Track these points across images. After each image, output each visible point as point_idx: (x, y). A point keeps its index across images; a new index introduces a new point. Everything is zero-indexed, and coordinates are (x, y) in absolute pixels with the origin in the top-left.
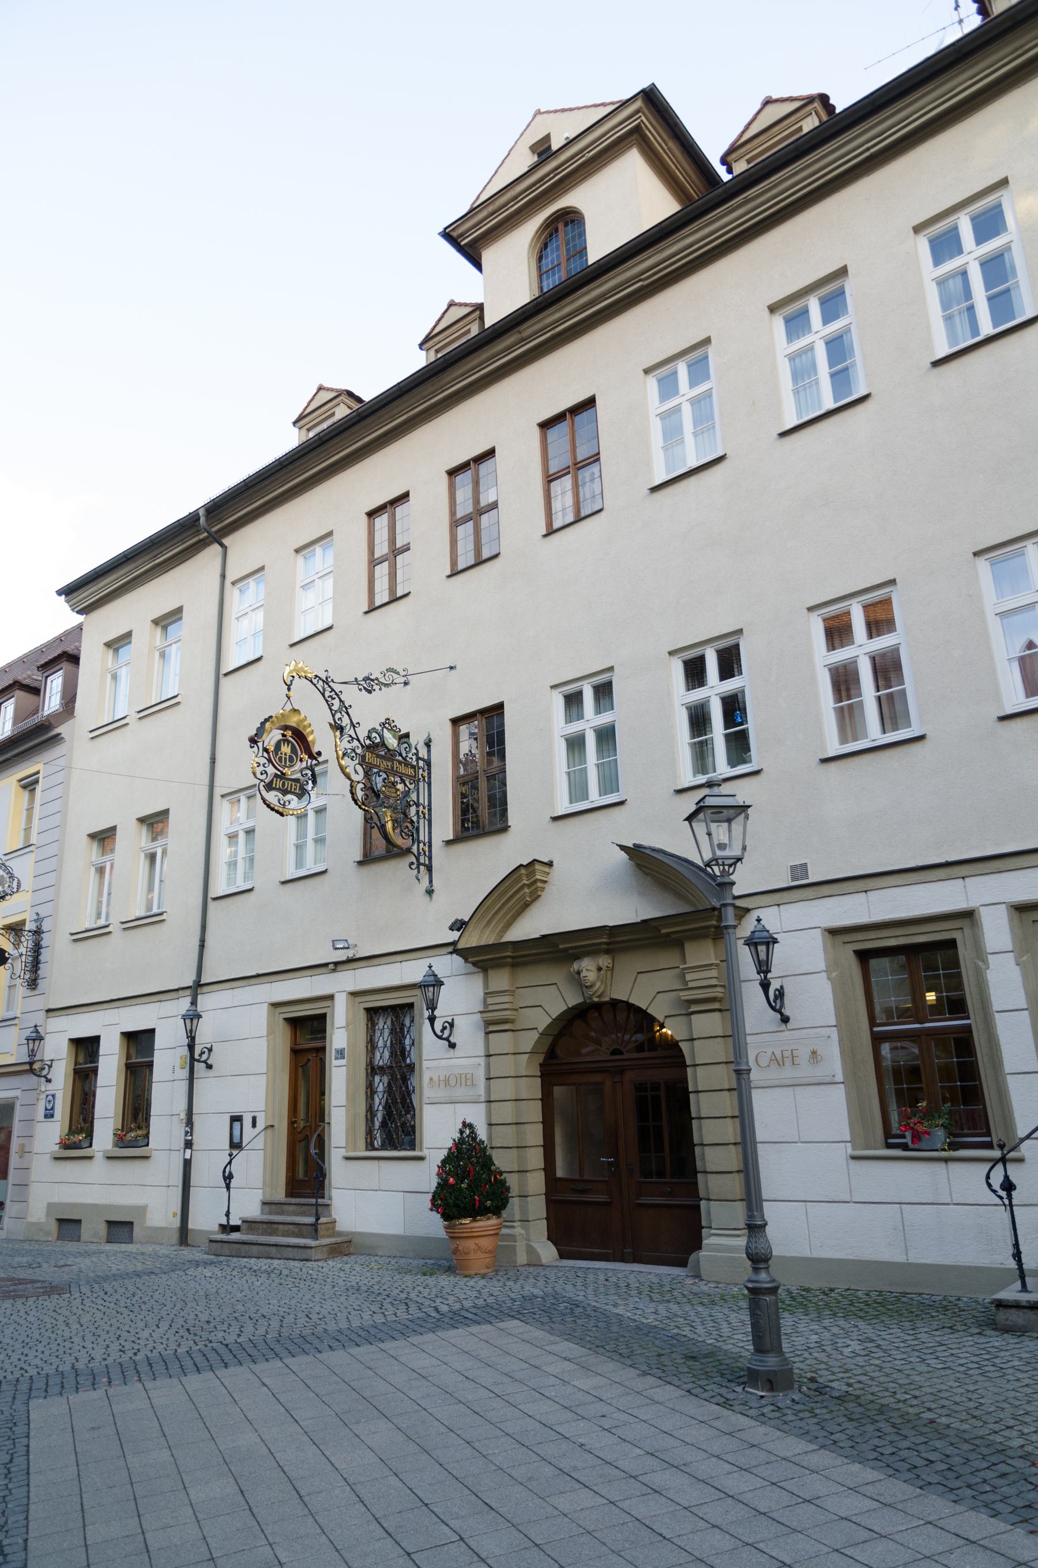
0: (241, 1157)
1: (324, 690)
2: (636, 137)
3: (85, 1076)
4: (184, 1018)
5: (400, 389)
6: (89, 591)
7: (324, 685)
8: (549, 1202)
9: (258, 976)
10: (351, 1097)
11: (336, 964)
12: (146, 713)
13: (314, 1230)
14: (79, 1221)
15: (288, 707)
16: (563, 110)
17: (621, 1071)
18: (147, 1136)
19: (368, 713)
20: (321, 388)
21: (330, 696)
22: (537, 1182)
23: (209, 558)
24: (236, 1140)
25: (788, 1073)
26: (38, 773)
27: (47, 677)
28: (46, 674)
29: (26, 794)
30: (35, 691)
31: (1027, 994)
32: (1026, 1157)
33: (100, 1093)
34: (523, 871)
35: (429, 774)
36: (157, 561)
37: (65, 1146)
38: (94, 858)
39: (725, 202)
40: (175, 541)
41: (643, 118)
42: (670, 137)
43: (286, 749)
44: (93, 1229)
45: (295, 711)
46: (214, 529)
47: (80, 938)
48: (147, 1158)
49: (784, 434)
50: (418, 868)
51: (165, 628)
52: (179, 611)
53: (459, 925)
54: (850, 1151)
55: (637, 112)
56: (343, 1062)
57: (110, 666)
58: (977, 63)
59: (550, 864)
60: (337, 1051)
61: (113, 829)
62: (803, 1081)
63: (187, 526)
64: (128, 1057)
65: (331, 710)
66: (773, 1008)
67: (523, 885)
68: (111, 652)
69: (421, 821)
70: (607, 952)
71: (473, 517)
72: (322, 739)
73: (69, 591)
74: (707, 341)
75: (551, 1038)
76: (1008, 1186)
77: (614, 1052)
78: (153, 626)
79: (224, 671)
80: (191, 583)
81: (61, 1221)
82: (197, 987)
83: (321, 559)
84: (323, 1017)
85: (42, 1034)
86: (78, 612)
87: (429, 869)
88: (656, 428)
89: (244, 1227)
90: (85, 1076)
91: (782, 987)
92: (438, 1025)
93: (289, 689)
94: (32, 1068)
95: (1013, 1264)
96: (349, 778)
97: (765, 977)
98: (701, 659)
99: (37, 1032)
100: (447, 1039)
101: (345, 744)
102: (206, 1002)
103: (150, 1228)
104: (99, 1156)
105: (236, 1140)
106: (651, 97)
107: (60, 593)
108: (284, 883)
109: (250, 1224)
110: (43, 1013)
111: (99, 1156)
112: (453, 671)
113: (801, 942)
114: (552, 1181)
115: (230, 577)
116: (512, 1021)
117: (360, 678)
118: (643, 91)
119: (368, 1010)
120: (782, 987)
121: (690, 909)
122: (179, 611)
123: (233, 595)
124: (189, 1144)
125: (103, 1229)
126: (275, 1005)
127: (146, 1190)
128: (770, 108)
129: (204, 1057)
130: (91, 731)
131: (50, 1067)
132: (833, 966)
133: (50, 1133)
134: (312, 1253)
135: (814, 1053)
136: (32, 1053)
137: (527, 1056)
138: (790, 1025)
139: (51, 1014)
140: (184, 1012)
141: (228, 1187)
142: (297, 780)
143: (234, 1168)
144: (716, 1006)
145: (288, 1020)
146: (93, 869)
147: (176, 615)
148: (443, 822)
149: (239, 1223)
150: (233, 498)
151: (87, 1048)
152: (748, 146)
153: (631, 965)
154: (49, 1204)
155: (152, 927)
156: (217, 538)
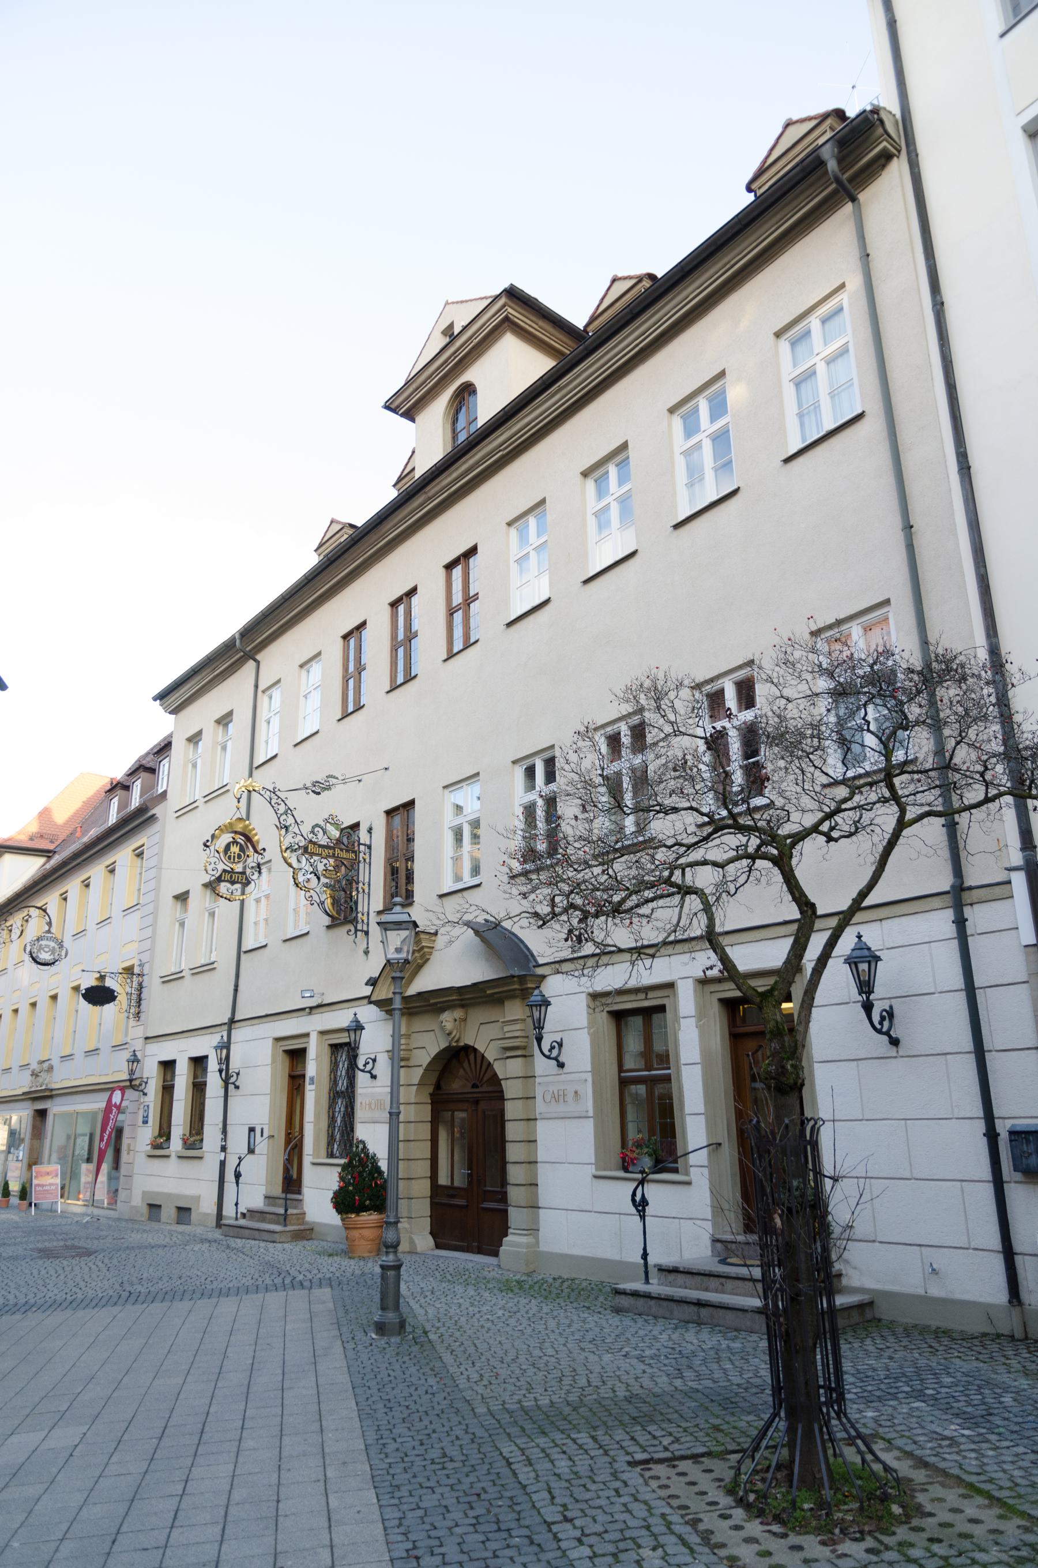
2: (507, 324)
5: (379, 517)
6: (177, 695)
8: (433, 1205)
9: (267, 1016)
10: (317, 1115)
11: (311, 1008)
14: (160, 1206)
16: (462, 302)
18: (202, 1140)
19: (311, 812)
22: (424, 1187)
24: (252, 1147)
25: (562, 1108)
26: (143, 845)
29: (139, 860)
31: (701, 1051)
32: (693, 1181)
37: (156, 1146)
38: (207, 905)
39: (592, 353)
41: (510, 310)
43: (234, 849)
44: (168, 1213)
48: (201, 1158)
49: (677, 526)
53: (373, 982)
54: (594, 1171)
55: (504, 306)
56: (313, 1087)
57: (220, 739)
61: (187, 892)
62: (569, 1115)
63: (227, 649)
66: (879, 1031)
68: (221, 727)
69: (361, 896)
70: (463, 1006)
71: (404, 642)
73: (162, 697)
74: (722, 374)
77: (474, 1086)
79: (255, 765)
80: (234, 692)
81: (151, 1206)
83: (316, 668)
85: (139, 1057)
86: (170, 713)
87: (367, 933)
88: (680, 463)
91: (891, 1007)
92: (546, 1046)
94: (133, 1084)
95: (642, 1261)
97: (868, 998)
98: (721, 692)
99: (135, 1055)
100: (556, 1059)
101: (288, 840)
102: (239, 1034)
104: (173, 1155)
106: (513, 294)
107: (155, 699)
108: (285, 941)
110: (142, 1040)
111: (173, 1155)
113: (569, 1006)
114: (436, 1189)
115: (262, 686)
116: (408, 1059)
117: (309, 785)
118: (505, 290)
119: (331, 1046)
120: (891, 1007)
123: (263, 700)
124: (224, 1149)
125: (173, 1212)
126: (278, 1040)
127: (188, 1181)
128: (791, 129)
129: (369, 1067)
131: (146, 1083)
132: (591, 1023)
133: (147, 1134)
134: (277, 1237)
135: (576, 1092)
136: (132, 1072)
138: (566, 1069)
139: (148, 1041)
140: (215, 1044)
141: (237, 1183)
143: (242, 1169)
144: (519, 1053)
146: (207, 914)
149: (245, 1211)
150: (259, 623)
151: (168, 1066)
154: (143, 1192)
155: (205, 975)
156: (251, 656)
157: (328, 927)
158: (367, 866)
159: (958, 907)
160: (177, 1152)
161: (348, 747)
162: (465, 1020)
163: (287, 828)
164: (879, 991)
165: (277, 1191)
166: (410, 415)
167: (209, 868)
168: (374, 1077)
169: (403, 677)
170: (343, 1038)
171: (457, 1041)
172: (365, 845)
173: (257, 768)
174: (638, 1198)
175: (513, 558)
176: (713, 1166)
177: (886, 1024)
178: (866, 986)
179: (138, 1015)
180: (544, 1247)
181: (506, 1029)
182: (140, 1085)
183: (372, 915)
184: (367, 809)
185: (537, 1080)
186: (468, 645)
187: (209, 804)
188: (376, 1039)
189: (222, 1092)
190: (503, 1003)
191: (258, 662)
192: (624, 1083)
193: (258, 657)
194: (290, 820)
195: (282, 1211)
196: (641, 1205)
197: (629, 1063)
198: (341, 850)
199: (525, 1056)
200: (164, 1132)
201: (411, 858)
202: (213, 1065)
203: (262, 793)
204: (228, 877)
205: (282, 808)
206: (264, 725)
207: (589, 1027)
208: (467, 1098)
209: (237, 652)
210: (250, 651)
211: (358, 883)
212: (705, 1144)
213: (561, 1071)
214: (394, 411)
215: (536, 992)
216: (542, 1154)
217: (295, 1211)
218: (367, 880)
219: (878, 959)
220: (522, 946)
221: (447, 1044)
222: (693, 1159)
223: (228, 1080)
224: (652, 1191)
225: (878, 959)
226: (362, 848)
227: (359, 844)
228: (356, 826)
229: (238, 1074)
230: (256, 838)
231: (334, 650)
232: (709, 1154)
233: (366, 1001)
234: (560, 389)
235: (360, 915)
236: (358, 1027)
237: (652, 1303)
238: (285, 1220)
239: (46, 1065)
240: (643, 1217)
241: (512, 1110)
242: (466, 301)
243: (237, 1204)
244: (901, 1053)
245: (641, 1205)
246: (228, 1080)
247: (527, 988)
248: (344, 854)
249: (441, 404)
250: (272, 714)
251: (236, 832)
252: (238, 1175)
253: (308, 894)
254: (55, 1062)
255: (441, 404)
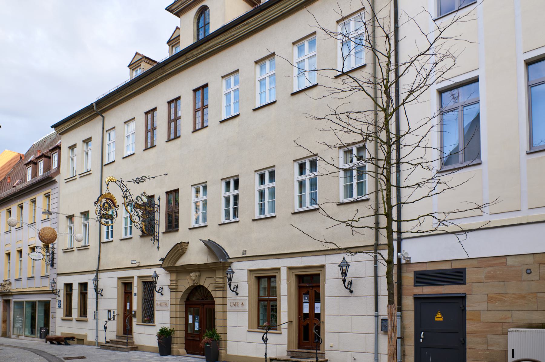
0: (109, 322)
3: (69, 295)
4: (93, 280)
7: (121, 183)
8: (186, 339)
12: (82, 176)
13: (126, 344)
17: (204, 305)
19: (136, 191)
20: (137, 53)
22: (183, 334)
33: (73, 301)
43: (107, 205)
45: (109, 193)
47: (66, 251)
52: (91, 138)
53: (162, 260)
59: (188, 243)
63: (89, 108)
66: (347, 288)
67: (180, 249)
70: (199, 271)
71: (174, 120)
72: (119, 200)
79: (104, 164)
80: (92, 129)
82: (98, 271)
83: (132, 125)
84: (131, 283)
87: (158, 240)
90: (69, 295)
92: (232, 287)
94: (54, 292)
100: (235, 292)
104: (74, 320)
107: (52, 127)
108: (121, 240)
109: (112, 341)
113: (241, 273)
115: (106, 129)
121: (220, 261)
122: (91, 138)
129: (160, 291)
132: (249, 279)
136: (53, 287)
141: (106, 331)
143: (107, 325)
146: (68, 228)
147: (90, 139)
148: (162, 227)
151: (69, 286)
153: (204, 276)
157: (141, 236)
161: (147, 162)
162: (200, 276)
163: (127, 197)
164: (348, 275)
165: (121, 334)
166: (178, 14)
167: (97, 213)
168: (162, 294)
169: (174, 136)
173: (105, 165)
174: (264, 338)
175: (224, 93)
176: (289, 328)
177: (349, 286)
178: (344, 274)
180: (228, 353)
184: (158, 190)
185: (228, 298)
186: (203, 127)
187: (82, 178)
191: (104, 117)
192: (259, 301)
193: (103, 115)
194: (128, 194)
195: (126, 341)
196: (265, 340)
204: (105, 216)
205: (125, 189)
206: (107, 146)
209: (94, 111)
211: (155, 220)
215: (229, 268)
216: (229, 323)
219: (349, 265)
222: (282, 326)
223: (98, 292)
224: (269, 336)
225: (349, 265)
226: (156, 206)
229: (102, 290)
231: (141, 119)
234: (248, 24)
239: (8, 282)
240: (266, 344)
241: (218, 308)
245: (265, 340)
246: (98, 292)
248: (149, 209)
249: (193, 12)
251: (107, 199)
252: (106, 328)
254: (12, 281)
255: (193, 12)
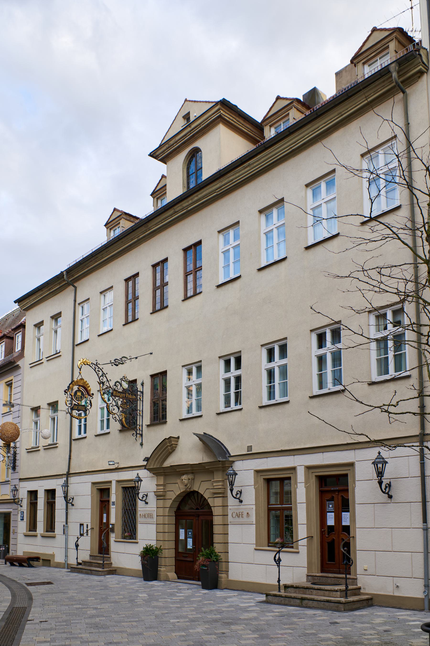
1: (95, 368)
2: (220, 119)
7: (96, 367)
15: (80, 377)
19: (114, 375)
21: (99, 371)
22: (172, 553)
23: (69, 291)
25: (241, 520)
26: (12, 380)
27: (16, 334)
28: (15, 333)
30: (12, 338)
34: (167, 441)
35: (143, 397)
36: (51, 291)
40: (56, 283)
41: (222, 112)
42: (236, 116)
43: (79, 394)
46: (70, 280)
47: (30, 451)
50: (136, 435)
51: (56, 320)
52: (60, 313)
53: (147, 459)
54: (255, 547)
55: (219, 109)
56: (114, 506)
58: (321, 121)
59: (178, 438)
60: (112, 502)
64: (48, 499)
65: (98, 376)
67: (168, 446)
70: (192, 473)
71: (160, 287)
72: (94, 387)
75: (178, 503)
76: (279, 560)
78: (51, 319)
79: (76, 343)
80: (62, 303)
82: (68, 474)
83: (110, 296)
85: (18, 488)
87: (142, 435)
89: (83, 563)
90: (33, 505)
91: (390, 482)
92: (234, 493)
93: (80, 370)
94: (15, 501)
95: (277, 584)
96: (106, 403)
97: (381, 479)
99: (16, 487)
100: (239, 499)
103: (56, 562)
104: (39, 535)
105: (82, 533)
108: (96, 436)
109: (85, 563)
110: (18, 480)
112: (152, 355)
113: (245, 474)
115: (78, 301)
120: (390, 482)
121: (218, 460)
122: (60, 313)
129: (144, 499)
130: (30, 364)
131: (22, 501)
132: (256, 482)
135: (248, 513)
136: (14, 496)
137: (168, 509)
138: (243, 504)
141: (77, 549)
142: (84, 406)
143: (79, 543)
145: (123, 488)
146: (33, 423)
147: (59, 315)
149: (81, 562)
151: (33, 494)
152: (270, 120)
153: (199, 479)
154: (24, 552)
158: (141, 402)
159: (422, 442)
160: (41, 534)
162: (193, 479)
163: (103, 383)
164: (386, 475)
168: (147, 503)
169: (160, 306)
170: (132, 484)
171: (190, 489)
172: (140, 391)
173: (77, 345)
174: (277, 558)
176: (309, 546)
177: (387, 489)
178: (380, 474)
179: (14, 468)
181: (214, 484)
182: (19, 502)
183: (144, 427)
186: (196, 294)
188: (148, 484)
189: (64, 507)
190: (213, 472)
191: (76, 288)
192: (269, 510)
193: (75, 285)
194: (105, 379)
195: (102, 562)
196: (278, 561)
197: (272, 501)
198: (129, 394)
199: (223, 497)
200: (33, 526)
201: (165, 400)
202: (59, 494)
203: (91, 365)
204: (76, 407)
205: (101, 373)
206: (80, 322)
207: (255, 485)
208: (194, 514)
209: (64, 280)
210: (71, 281)
211: (137, 410)
212: (306, 537)
213: (241, 504)
214: (156, 158)
215: (230, 469)
216: (231, 539)
217: (108, 562)
218: (141, 409)
219: (386, 462)
220: (223, 447)
221: (185, 490)
222: (300, 543)
225: (386, 462)
226: (139, 393)
227: (138, 391)
228: (135, 381)
229: (73, 499)
230: (89, 388)
231: (120, 288)
232: (308, 541)
233: (144, 468)
234: (249, 165)
235: (138, 426)
236: (140, 480)
237: (282, 599)
238: (103, 566)
240: (279, 566)
241: (217, 520)
242: (197, 102)
243: (77, 558)
244: (392, 502)
245: (278, 561)
246: (69, 501)
247: (226, 467)
248: (130, 396)
249: (182, 157)
250: (84, 317)
251: (79, 386)
253: (114, 416)
255: (182, 157)
